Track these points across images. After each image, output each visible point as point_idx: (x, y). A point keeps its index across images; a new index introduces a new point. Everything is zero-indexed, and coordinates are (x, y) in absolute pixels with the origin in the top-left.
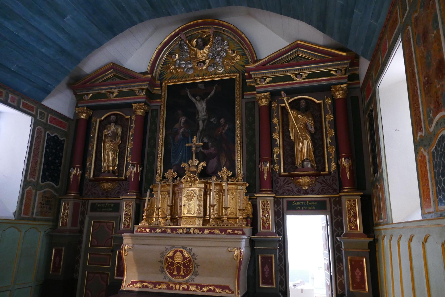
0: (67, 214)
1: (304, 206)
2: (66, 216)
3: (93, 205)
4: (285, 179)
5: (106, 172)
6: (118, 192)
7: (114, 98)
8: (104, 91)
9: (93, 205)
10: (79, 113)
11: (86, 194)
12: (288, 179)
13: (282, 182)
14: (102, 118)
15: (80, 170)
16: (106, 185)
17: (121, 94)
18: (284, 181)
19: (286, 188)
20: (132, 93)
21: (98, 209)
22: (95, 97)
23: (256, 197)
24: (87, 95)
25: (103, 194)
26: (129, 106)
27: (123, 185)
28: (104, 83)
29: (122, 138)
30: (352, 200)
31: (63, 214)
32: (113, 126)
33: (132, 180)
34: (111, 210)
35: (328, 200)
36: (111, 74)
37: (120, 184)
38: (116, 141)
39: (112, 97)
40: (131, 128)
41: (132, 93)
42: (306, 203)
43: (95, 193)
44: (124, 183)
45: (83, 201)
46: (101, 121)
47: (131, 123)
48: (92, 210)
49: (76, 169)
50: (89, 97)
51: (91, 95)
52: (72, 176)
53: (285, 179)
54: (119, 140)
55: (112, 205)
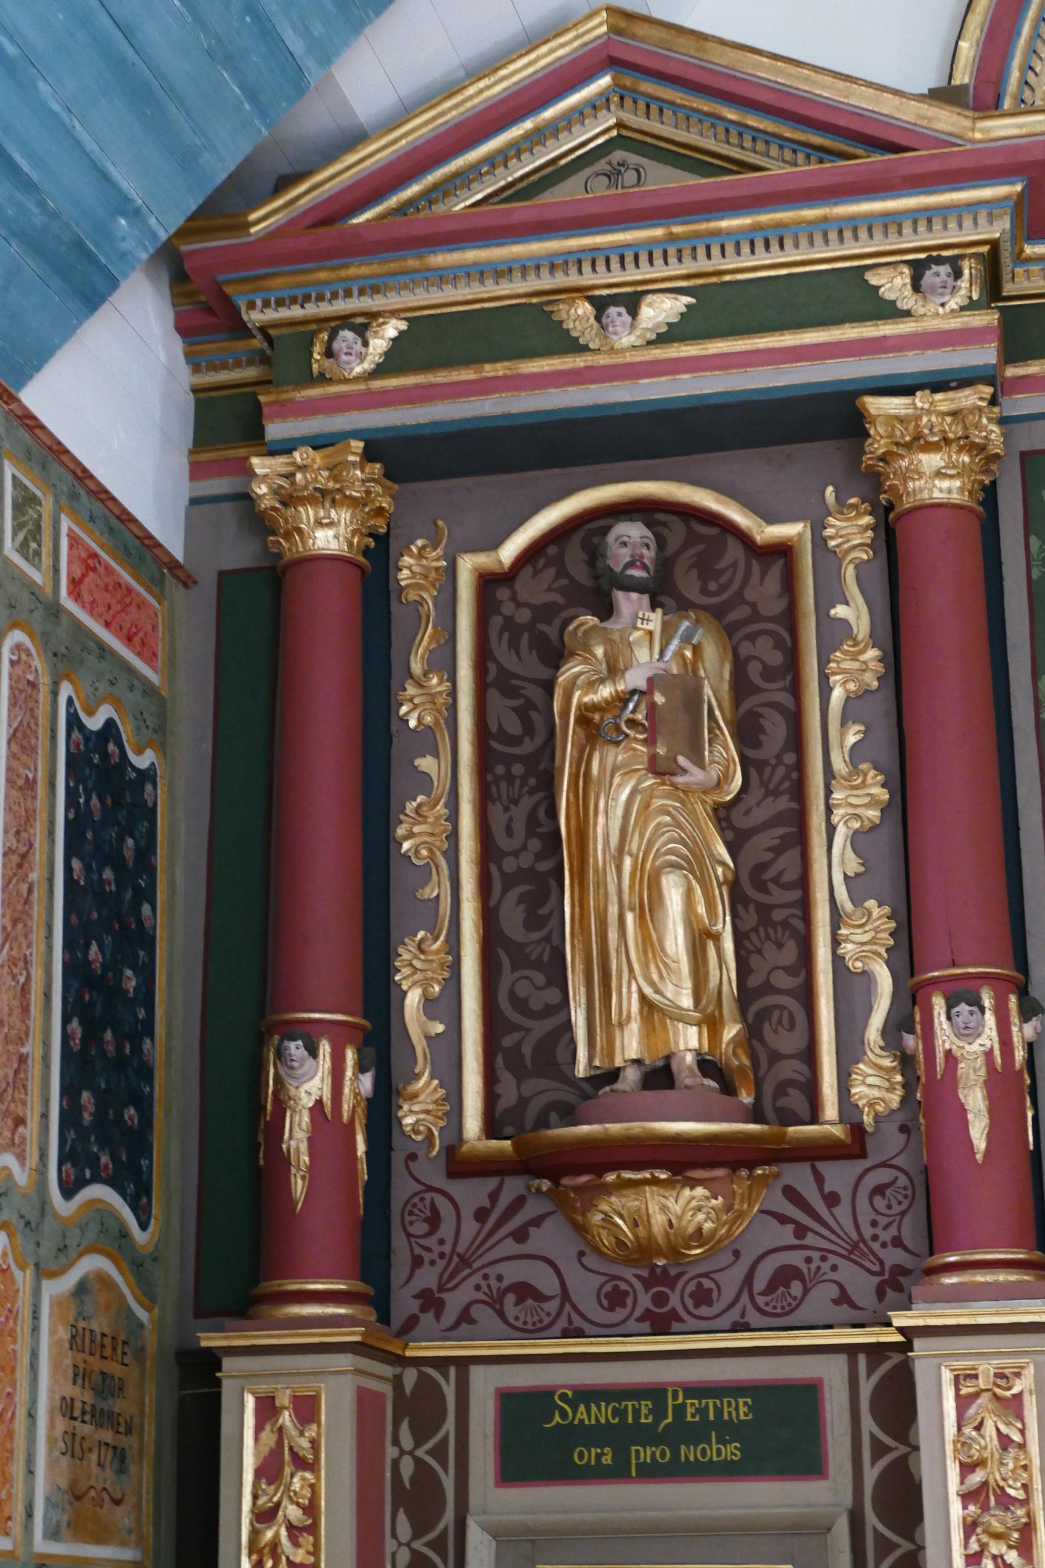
0: (311, 1509)
1: (645, 1435)
2: (304, 1530)
3: (520, 1410)
4: (494, 1196)
5: (631, 1076)
6: (784, 1276)
7: (640, 347)
8: (518, 286)
9: (520, 1410)
10: (289, 500)
11: (431, 1302)
12: (513, 1186)
13: (470, 1227)
14: (509, 551)
15: (361, 1068)
16: (682, 1208)
17: (719, 309)
18: (481, 1215)
19: (514, 1273)
20: (848, 295)
21: (585, 1456)
22: (432, 342)
23: (901, 1330)
24: (362, 325)
25: (615, 1299)
26: (832, 419)
27: (832, 1200)
28: (524, 207)
29: (747, 732)
30: (986, 1369)
31: (265, 1516)
32: (639, 620)
33: (980, 1142)
34: (731, 1451)
35: (832, 1373)
36: (586, 119)
37: (791, 1194)
38: (700, 763)
39: (627, 340)
40: (832, 634)
41: (848, 295)
42: (659, 1411)
43: (524, 1291)
44: (839, 1176)
45: (410, 1377)
46: (488, 583)
47: (830, 592)
48: (513, 1469)
49: (325, 1048)
50: (379, 345)
51: (392, 329)
52: (297, 1135)
53: (494, 1196)
54: (722, 764)
55: (741, 1410)
